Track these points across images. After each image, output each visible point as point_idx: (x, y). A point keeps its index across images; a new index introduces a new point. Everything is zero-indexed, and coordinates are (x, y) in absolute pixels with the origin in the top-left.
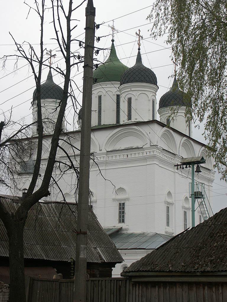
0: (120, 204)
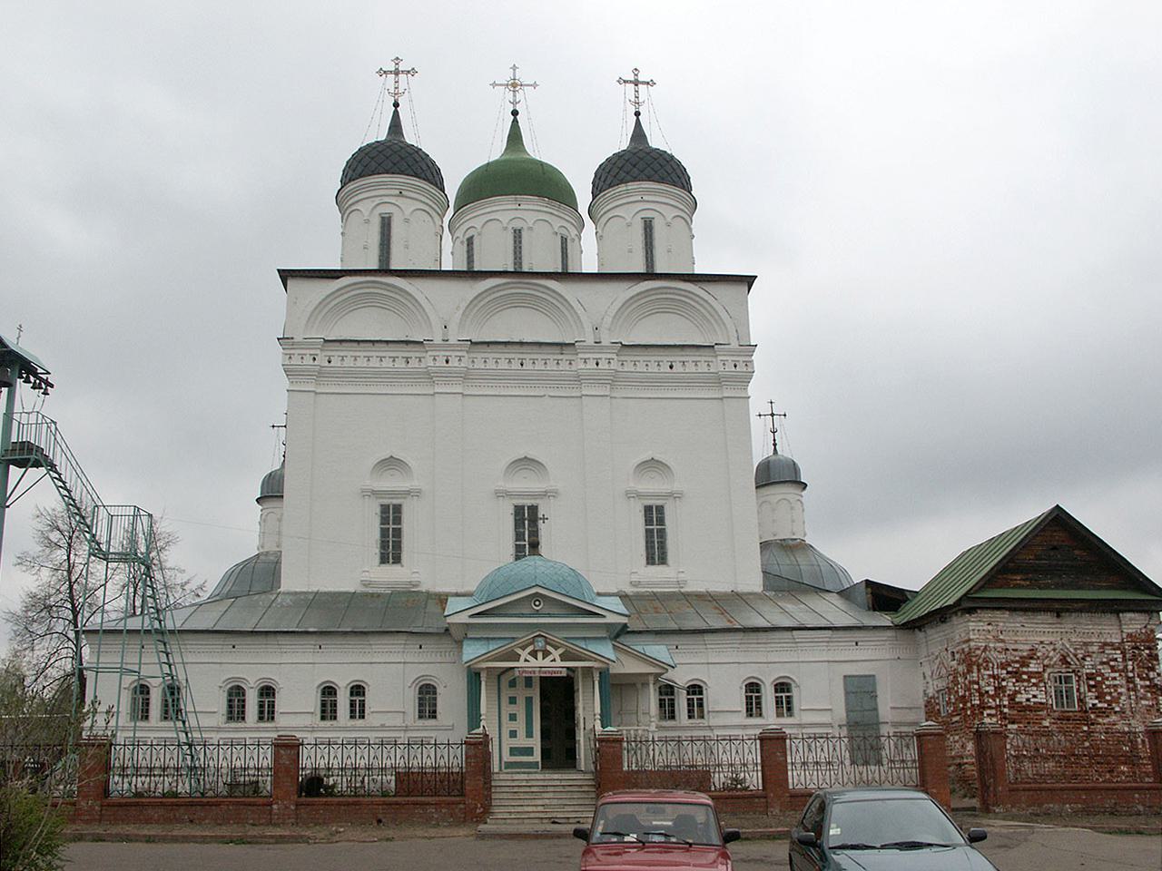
0: (385, 509)
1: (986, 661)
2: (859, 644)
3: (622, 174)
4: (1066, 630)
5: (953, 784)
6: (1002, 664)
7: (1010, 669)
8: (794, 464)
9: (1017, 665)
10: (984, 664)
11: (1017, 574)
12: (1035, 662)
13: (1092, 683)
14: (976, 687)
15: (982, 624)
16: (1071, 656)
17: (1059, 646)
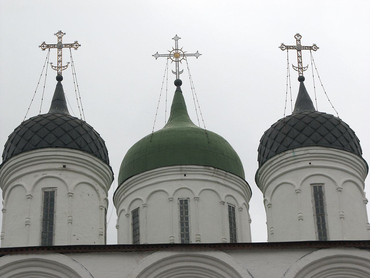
3: (288, 140)
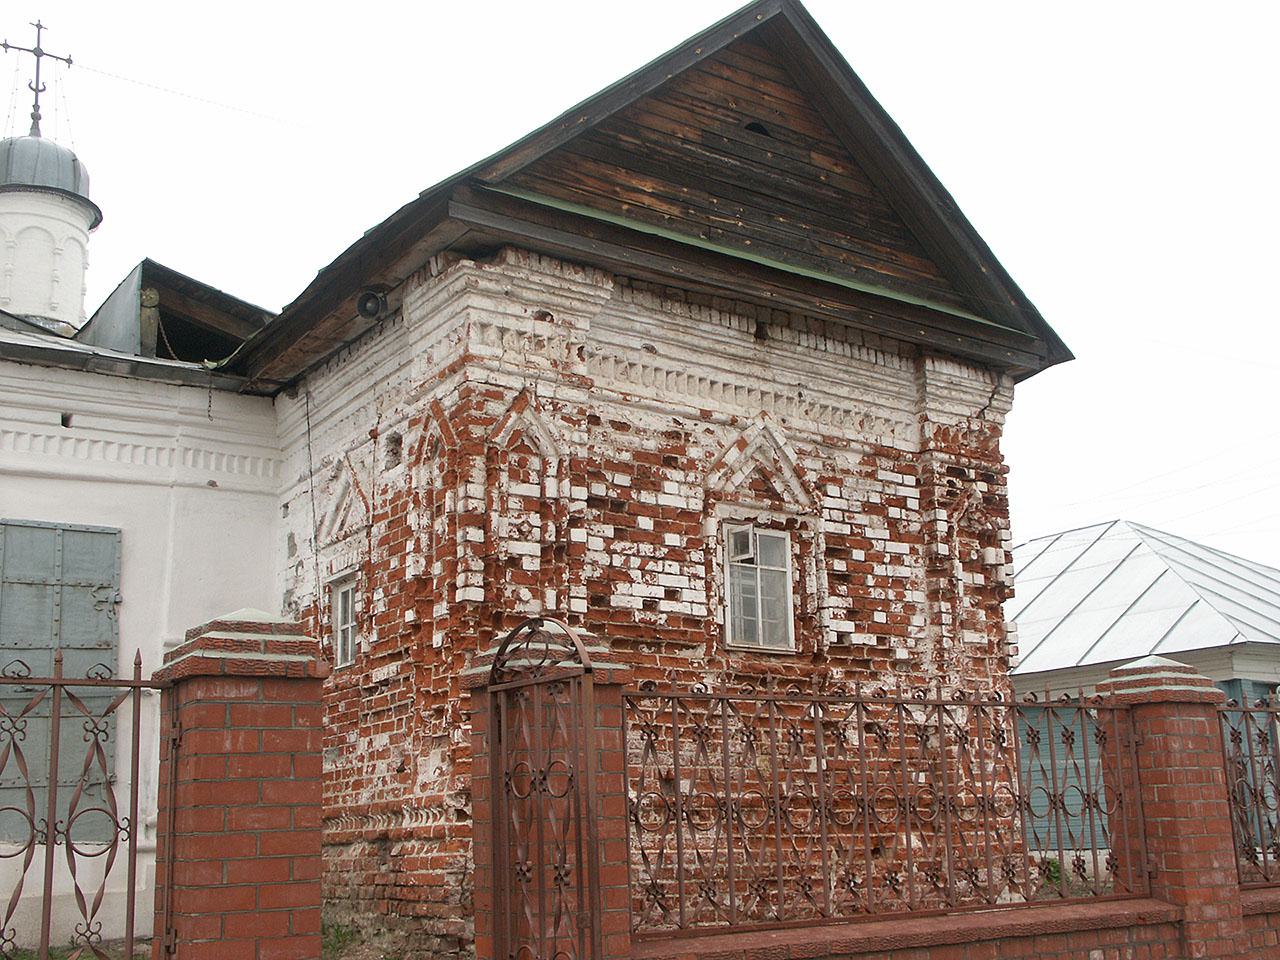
1: (523, 444)
2: (75, 420)
4: (778, 388)
5: (355, 908)
6: (574, 462)
7: (599, 489)
8: (75, 160)
9: (623, 480)
10: (514, 457)
11: (644, 172)
12: (678, 475)
13: (840, 566)
14: (476, 535)
15: (517, 309)
16: (788, 473)
17: (753, 434)
